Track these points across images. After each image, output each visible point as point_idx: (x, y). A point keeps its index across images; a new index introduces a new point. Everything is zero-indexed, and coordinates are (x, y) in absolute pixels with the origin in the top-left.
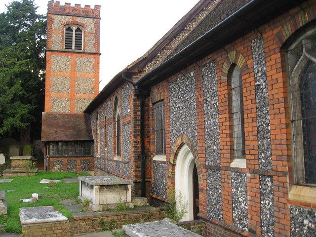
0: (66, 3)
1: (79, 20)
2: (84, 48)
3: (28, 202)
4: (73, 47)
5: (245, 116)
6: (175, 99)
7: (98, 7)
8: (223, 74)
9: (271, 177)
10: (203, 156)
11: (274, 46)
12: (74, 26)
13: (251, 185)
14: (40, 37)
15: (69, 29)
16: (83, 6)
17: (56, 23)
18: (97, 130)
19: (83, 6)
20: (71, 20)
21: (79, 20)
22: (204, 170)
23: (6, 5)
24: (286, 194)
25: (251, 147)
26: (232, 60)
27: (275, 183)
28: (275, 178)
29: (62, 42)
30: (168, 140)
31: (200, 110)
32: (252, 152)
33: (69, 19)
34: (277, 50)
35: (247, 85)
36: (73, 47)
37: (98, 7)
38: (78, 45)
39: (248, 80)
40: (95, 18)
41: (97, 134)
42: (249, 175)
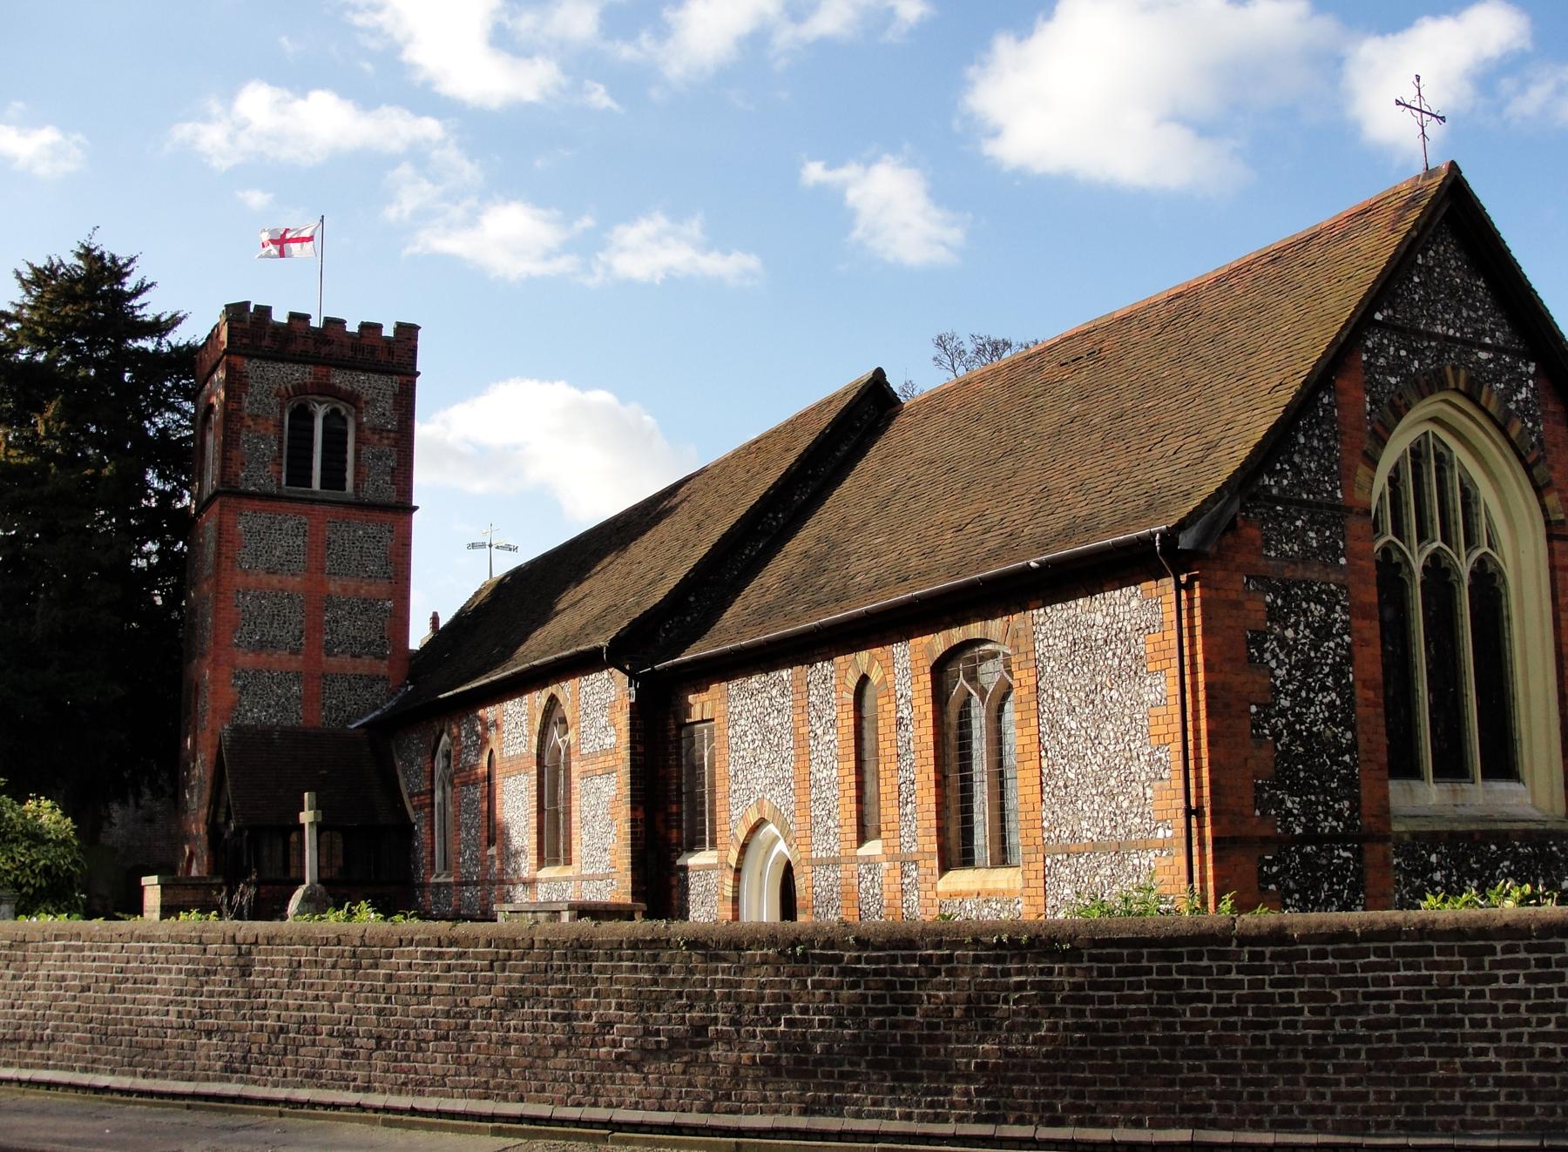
0: (293, 316)
1: (339, 379)
2: (356, 486)
3: (1529, 461)
4: (316, 484)
5: (881, 767)
6: (743, 722)
7: (408, 333)
8: (847, 690)
9: (915, 862)
10: (807, 840)
11: (923, 663)
12: (320, 403)
13: (890, 880)
14: (154, 424)
15: (302, 418)
16: (352, 327)
17: (255, 389)
18: (432, 791)
19: (352, 327)
20: (309, 379)
21: (339, 379)
22: (808, 869)
23: (19, 275)
24: (934, 885)
25: (889, 818)
26: (864, 669)
27: (922, 871)
28: (921, 863)
29: (276, 460)
30: (723, 815)
31: (800, 751)
32: (890, 826)
33: (299, 374)
34: (928, 670)
35: (885, 715)
36: (316, 484)
37: (408, 333)
38: (334, 476)
39: (887, 708)
40: (398, 374)
41: (432, 805)
42: (886, 865)
